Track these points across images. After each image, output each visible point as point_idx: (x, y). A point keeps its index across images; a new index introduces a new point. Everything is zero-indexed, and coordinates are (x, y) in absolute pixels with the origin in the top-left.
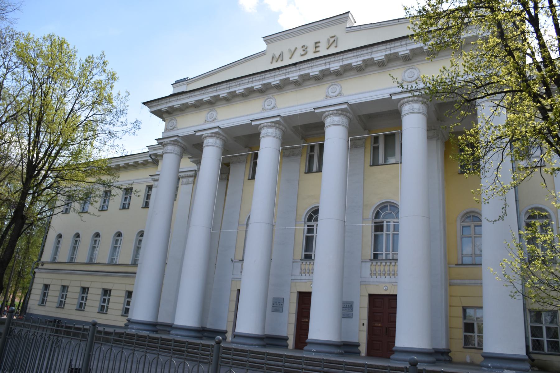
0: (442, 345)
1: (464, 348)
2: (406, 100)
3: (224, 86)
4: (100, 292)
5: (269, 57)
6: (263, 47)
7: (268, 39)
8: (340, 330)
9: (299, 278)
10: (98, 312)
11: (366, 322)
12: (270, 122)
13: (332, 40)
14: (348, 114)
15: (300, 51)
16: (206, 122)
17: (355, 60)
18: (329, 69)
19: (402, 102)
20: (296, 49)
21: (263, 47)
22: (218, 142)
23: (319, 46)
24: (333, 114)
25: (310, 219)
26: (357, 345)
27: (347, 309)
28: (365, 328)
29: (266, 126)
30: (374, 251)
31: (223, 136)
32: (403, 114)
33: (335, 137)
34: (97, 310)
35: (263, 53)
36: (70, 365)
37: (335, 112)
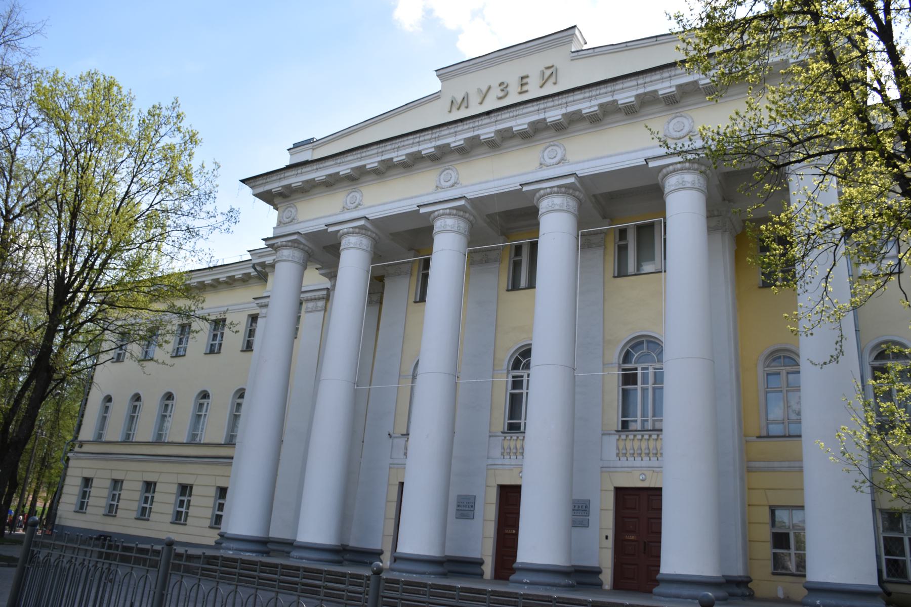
2: (671, 168)
3: (374, 150)
7: (444, 73)
12: (449, 208)
13: (548, 73)
14: (577, 193)
15: (496, 92)
16: (345, 209)
17: (588, 104)
18: (545, 119)
19: (664, 171)
20: (489, 88)
21: (435, 85)
23: (526, 84)
29: (443, 214)
31: (372, 231)
32: (666, 190)
33: (556, 231)
37: (556, 189)
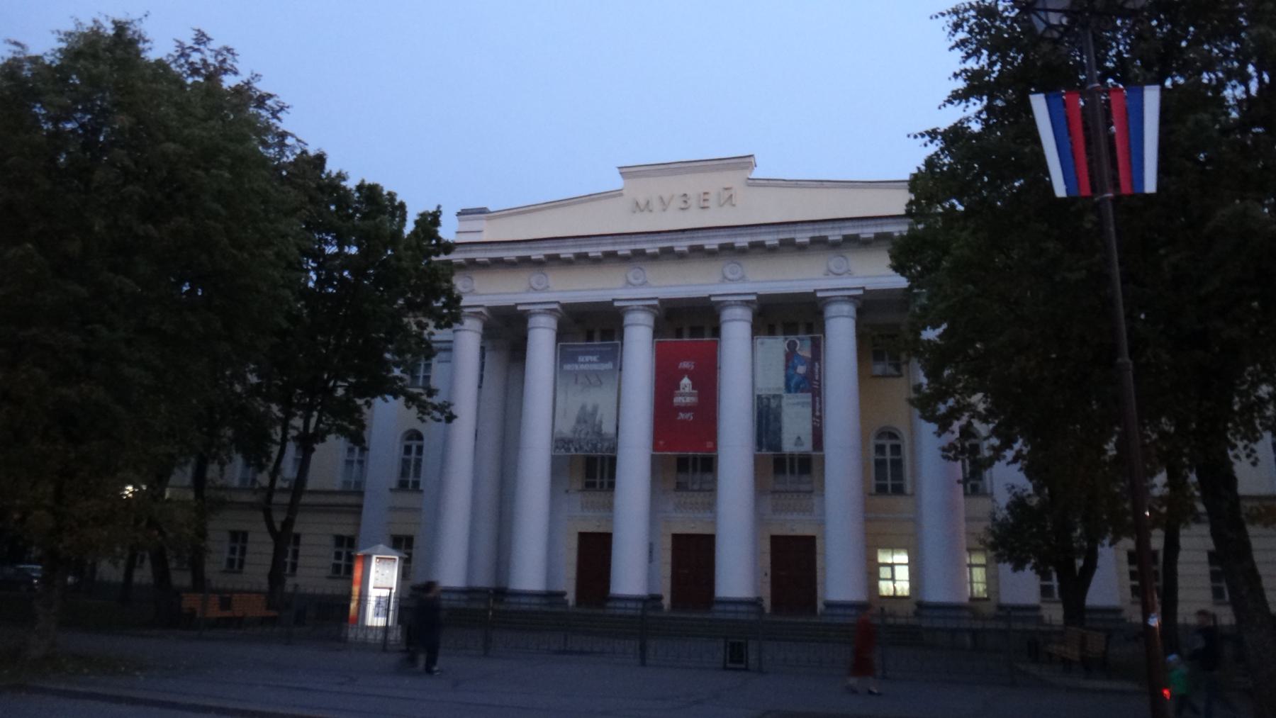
7: (627, 172)
35: (617, 194)
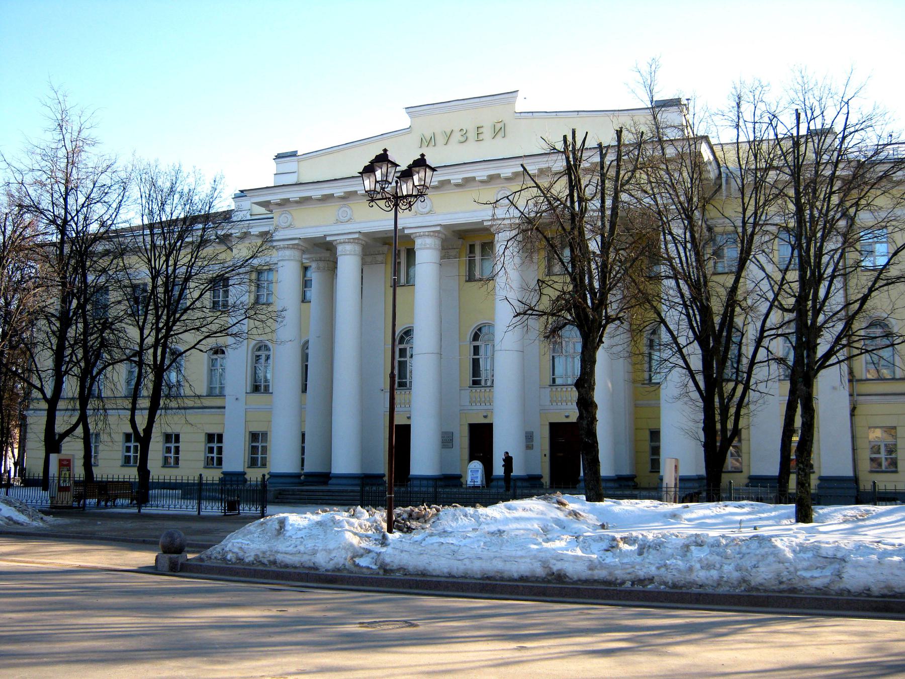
0: (626, 471)
1: (651, 472)
4: (202, 438)
5: (415, 138)
6: (404, 122)
8: (442, 462)
9: (469, 408)
10: (122, 466)
11: (547, 452)
16: (338, 222)
21: (404, 122)
22: (357, 249)
24: (349, 242)
25: (476, 337)
26: (539, 477)
27: (447, 440)
28: (547, 459)
30: (473, 376)
34: (120, 463)
36: (772, 536)
